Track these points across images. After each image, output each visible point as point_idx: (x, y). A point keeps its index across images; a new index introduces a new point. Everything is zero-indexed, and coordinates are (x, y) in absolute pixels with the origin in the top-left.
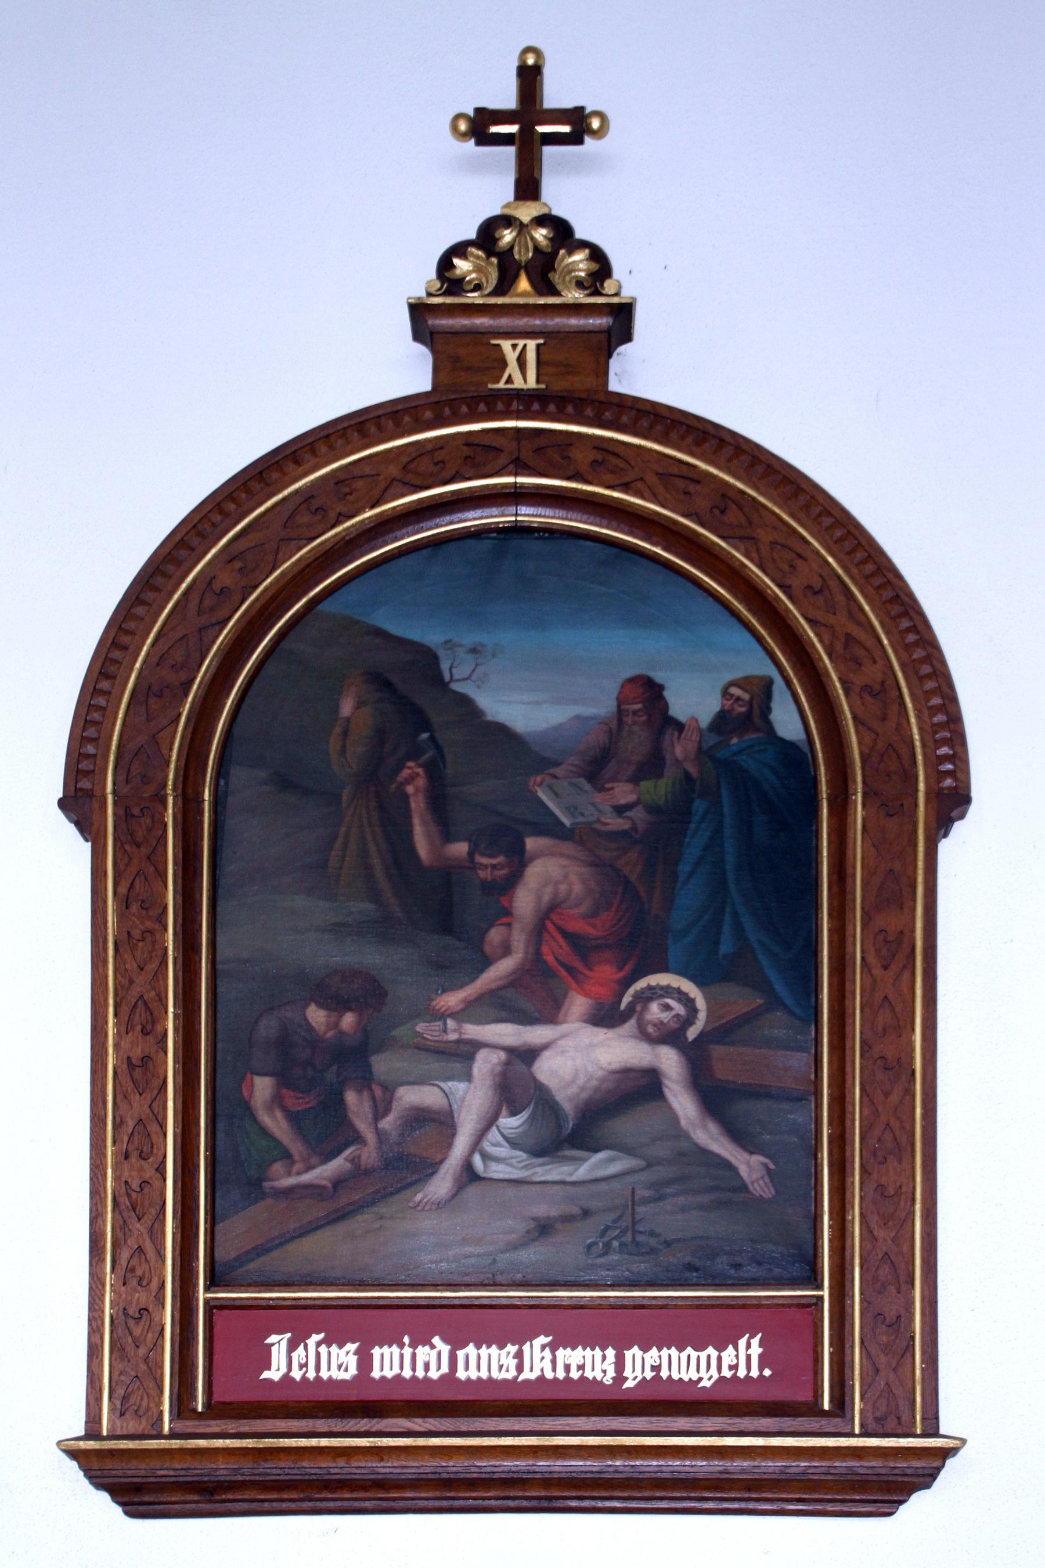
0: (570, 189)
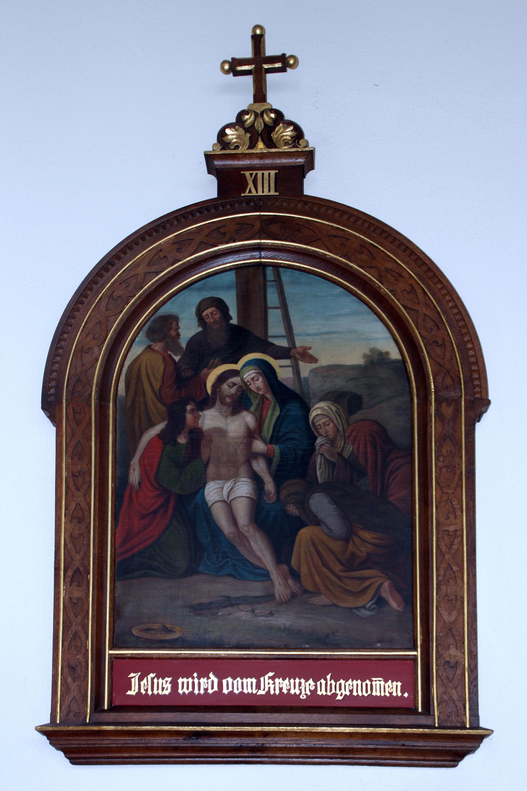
0: (284, 94)
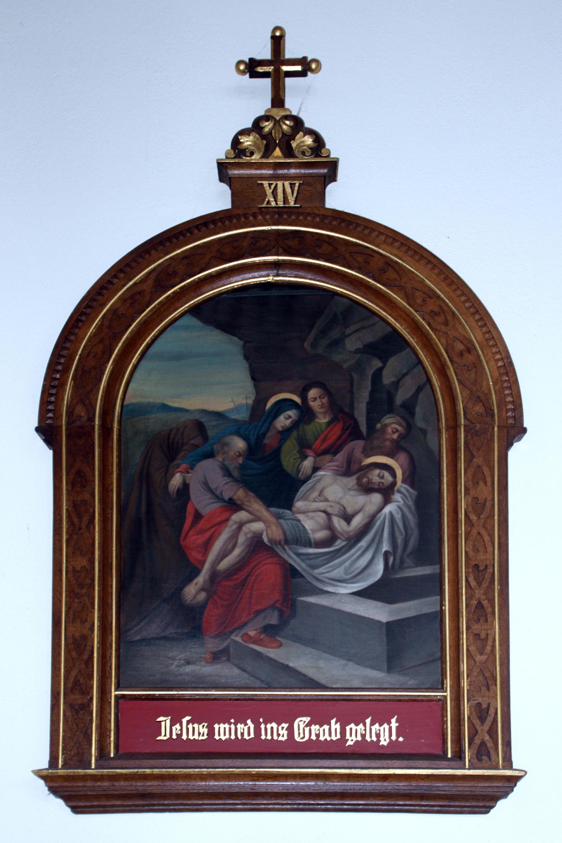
0: (301, 98)
